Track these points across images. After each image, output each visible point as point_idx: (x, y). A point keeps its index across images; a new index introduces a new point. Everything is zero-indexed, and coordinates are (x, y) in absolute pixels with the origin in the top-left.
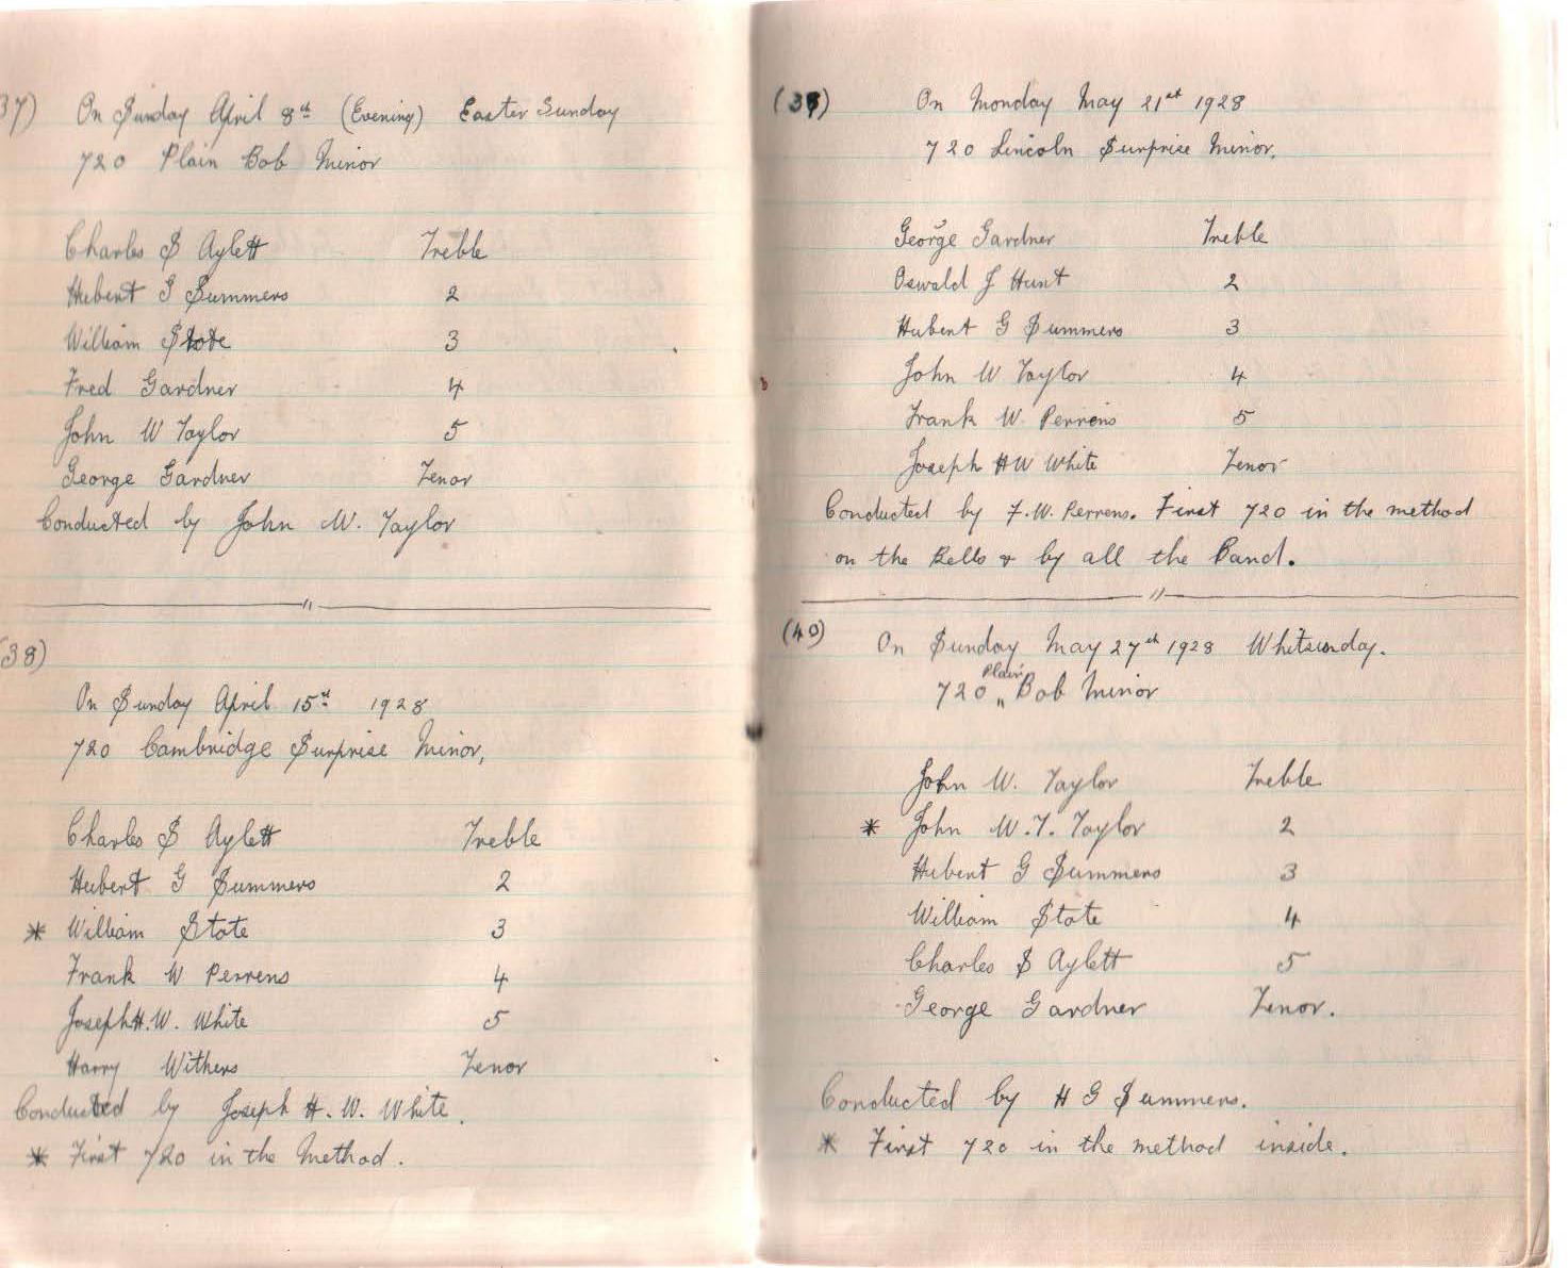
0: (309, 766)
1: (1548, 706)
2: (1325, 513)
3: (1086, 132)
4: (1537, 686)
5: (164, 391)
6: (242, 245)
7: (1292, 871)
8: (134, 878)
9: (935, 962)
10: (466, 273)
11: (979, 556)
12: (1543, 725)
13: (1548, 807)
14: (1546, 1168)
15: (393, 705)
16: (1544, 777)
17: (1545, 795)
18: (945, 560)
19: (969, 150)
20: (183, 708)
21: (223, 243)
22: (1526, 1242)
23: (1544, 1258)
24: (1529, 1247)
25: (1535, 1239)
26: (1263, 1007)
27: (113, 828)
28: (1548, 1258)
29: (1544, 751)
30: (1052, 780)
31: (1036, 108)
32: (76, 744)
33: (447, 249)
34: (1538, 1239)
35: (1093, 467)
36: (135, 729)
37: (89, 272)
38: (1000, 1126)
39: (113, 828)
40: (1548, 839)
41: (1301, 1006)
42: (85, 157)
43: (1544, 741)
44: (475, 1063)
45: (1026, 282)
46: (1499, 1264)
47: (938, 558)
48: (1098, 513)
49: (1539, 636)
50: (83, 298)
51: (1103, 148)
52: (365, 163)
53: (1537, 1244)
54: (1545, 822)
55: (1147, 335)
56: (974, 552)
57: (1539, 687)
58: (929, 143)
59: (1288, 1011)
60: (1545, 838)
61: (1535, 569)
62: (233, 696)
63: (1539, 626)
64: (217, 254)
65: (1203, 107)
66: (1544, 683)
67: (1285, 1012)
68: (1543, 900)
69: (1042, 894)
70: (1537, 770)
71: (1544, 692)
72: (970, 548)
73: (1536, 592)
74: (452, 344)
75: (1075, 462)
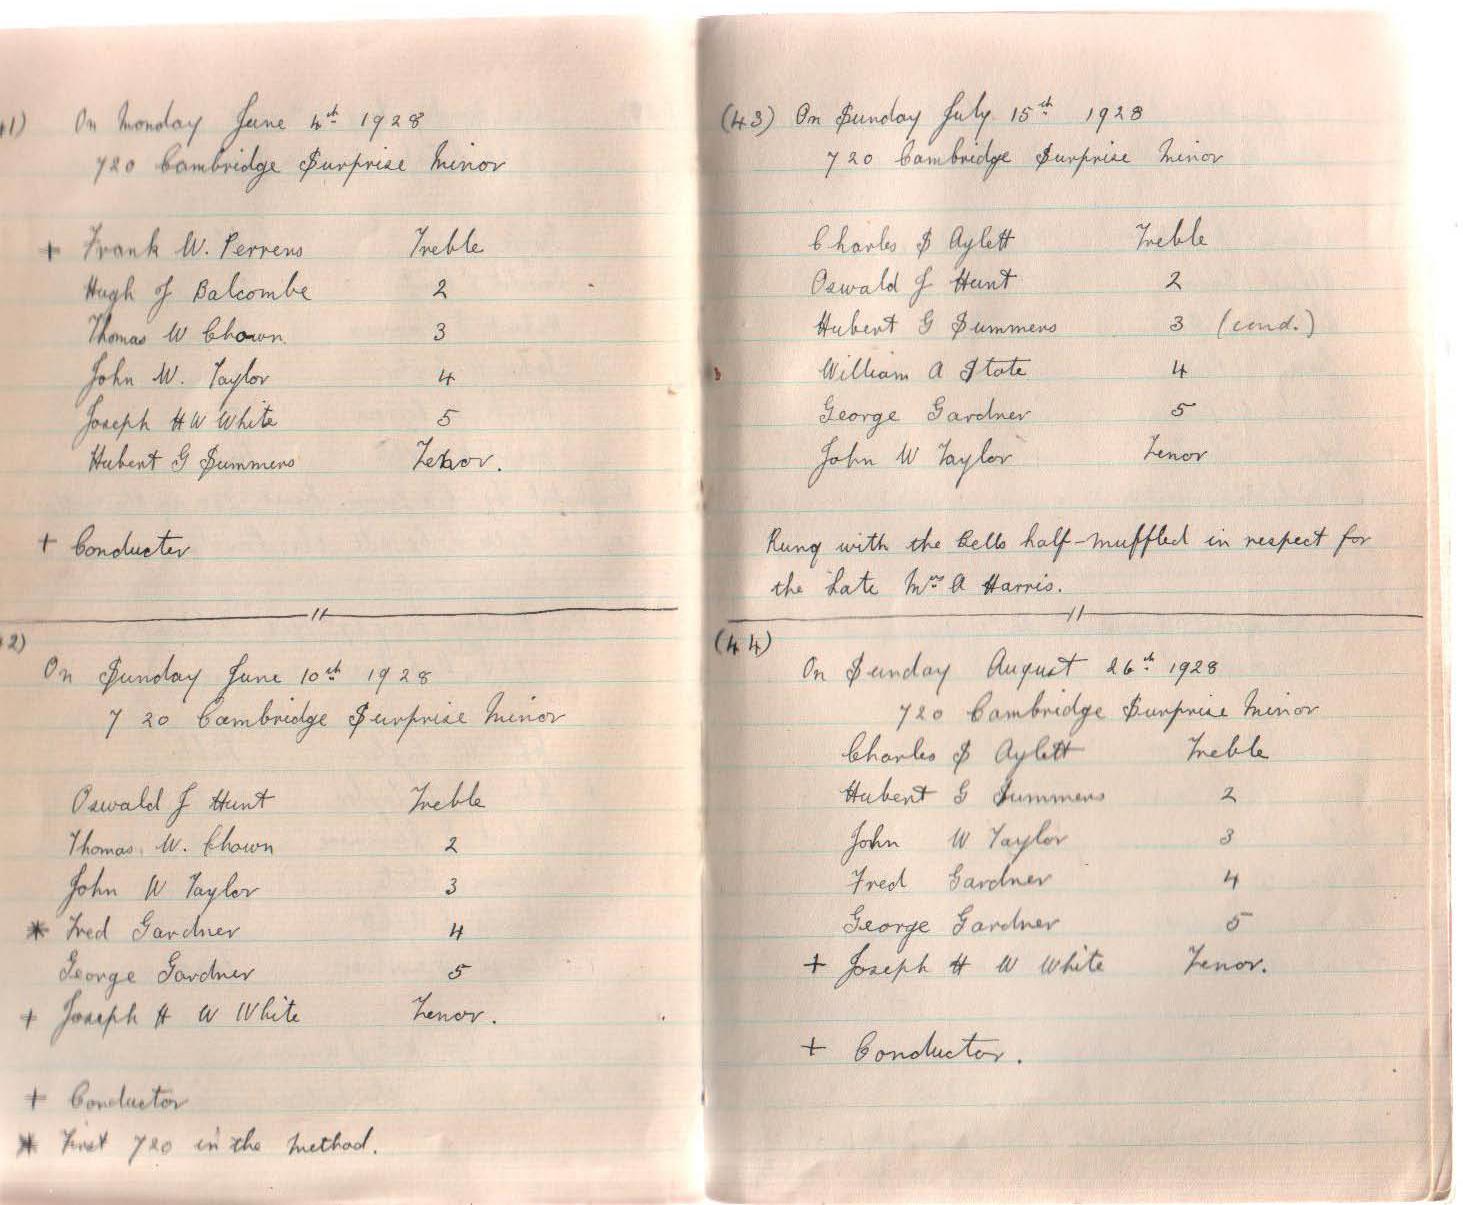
3: (1020, 142)
4: (1438, 657)
5: (222, 382)
6: (994, 238)
7: (1230, 836)
9: (133, 1015)
11: (1000, 541)
12: (1445, 692)
14: (1450, 1108)
16: (1446, 741)
17: (1446, 758)
18: (969, 543)
19: (868, 159)
21: (973, 234)
22: (1429, 1179)
25: (1439, 1174)
26: (1197, 961)
28: (1451, 1193)
31: (904, 123)
40: (1450, 799)
42: (102, 163)
44: (1200, 959)
45: (99, 292)
47: (962, 542)
50: (102, 293)
54: (1446, 781)
55: (1090, 339)
56: (995, 537)
57: (1440, 656)
58: (830, 154)
60: (1447, 798)
61: (1436, 546)
63: (1440, 599)
66: (1445, 652)
68: (1443, 858)
70: (1438, 735)
72: (1061, 528)
73: (1437, 568)
74: (440, 335)
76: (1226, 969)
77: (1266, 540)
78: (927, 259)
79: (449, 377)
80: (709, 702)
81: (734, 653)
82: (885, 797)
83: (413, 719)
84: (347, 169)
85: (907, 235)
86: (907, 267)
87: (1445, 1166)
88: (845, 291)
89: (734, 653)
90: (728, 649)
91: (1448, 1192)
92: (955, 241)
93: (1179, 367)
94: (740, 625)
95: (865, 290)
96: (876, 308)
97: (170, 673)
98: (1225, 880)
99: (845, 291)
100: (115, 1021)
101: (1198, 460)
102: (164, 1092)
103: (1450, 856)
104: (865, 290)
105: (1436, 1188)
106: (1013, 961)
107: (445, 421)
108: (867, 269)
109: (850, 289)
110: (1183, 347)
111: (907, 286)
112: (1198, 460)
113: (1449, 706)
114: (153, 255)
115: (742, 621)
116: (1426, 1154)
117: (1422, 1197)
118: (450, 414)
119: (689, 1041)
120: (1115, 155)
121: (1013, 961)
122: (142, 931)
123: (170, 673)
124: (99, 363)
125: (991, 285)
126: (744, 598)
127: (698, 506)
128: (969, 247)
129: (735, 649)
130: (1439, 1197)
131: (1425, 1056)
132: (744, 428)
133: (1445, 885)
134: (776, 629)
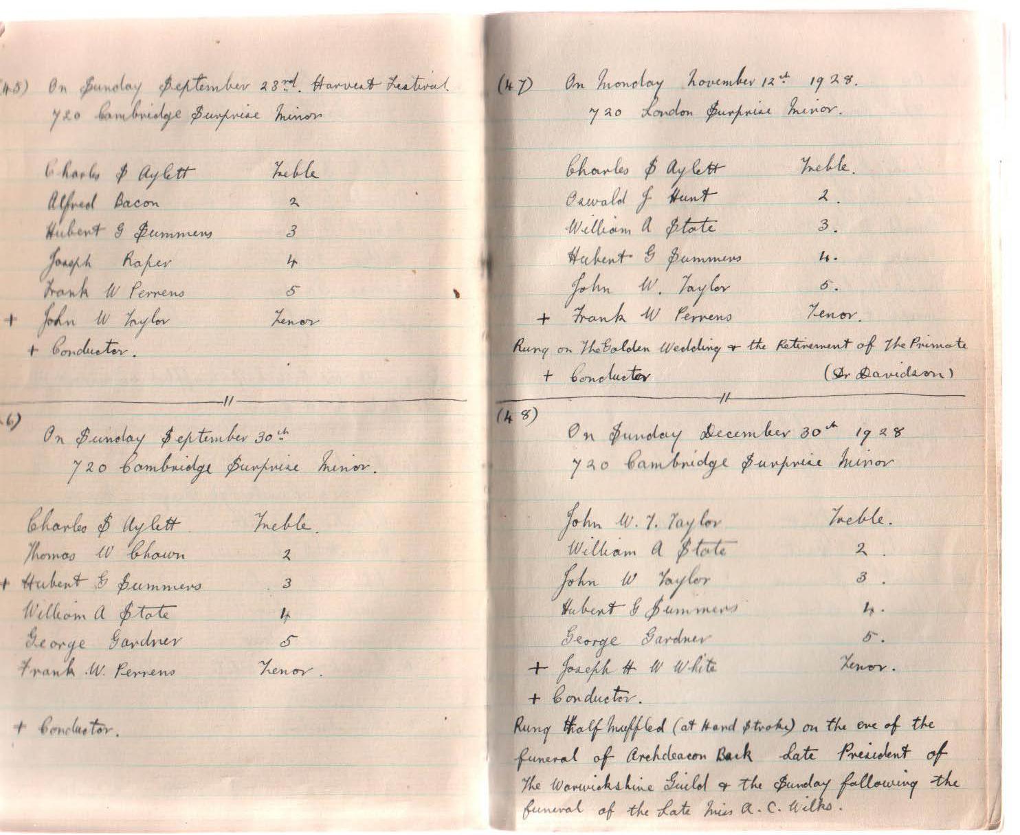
0: (242, 479)
1: (1000, 468)
2: (705, 756)
8: (77, 578)
10: (300, 187)
12: (997, 481)
13: (1001, 534)
14: (1000, 766)
16: (998, 514)
17: (998, 525)
24: (988, 818)
25: (992, 813)
30: (673, 520)
37: (65, 186)
42: (56, 114)
43: (998, 492)
46: (973, 829)
51: (162, 86)
52: (684, 112)
53: (994, 814)
54: (998, 542)
60: (999, 553)
63: (994, 416)
65: (816, 84)
69: (646, 626)
71: (998, 460)
78: (652, 180)
80: (491, 488)
81: (509, 422)
85: (637, 165)
86: (635, 185)
88: (591, 203)
89: (509, 422)
90: (505, 420)
91: (999, 823)
92: (671, 170)
94: (515, 403)
95: (604, 203)
96: (609, 216)
97: (124, 85)
98: (821, 259)
99: (591, 203)
102: (98, 724)
103: (1001, 593)
104: (604, 203)
105: (990, 822)
108: (607, 187)
109: (595, 201)
110: (826, 242)
111: (635, 199)
113: (1000, 490)
114: (84, 295)
115: (516, 401)
116: (984, 799)
117: (980, 827)
119: (478, 721)
123: (124, 85)
124: (49, 310)
126: (515, 266)
128: (681, 172)
129: (510, 420)
130: (992, 828)
131: (984, 729)
132: (519, 443)
133: (997, 613)
134: (540, 405)
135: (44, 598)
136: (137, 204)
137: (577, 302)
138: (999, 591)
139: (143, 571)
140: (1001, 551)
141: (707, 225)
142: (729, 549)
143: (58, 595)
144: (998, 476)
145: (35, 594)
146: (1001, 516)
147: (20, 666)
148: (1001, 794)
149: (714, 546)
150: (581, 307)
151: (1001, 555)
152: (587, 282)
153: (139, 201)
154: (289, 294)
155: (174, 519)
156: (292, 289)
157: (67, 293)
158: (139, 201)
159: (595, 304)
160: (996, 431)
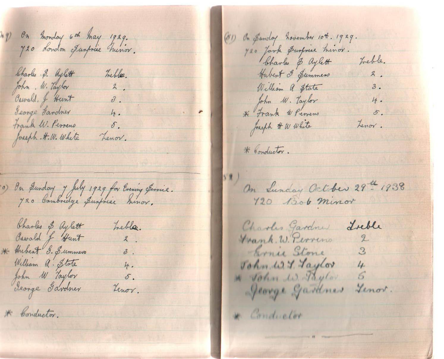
1: (433, 203)
12: (431, 208)
15: (344, 37)
16: (432, 223)
20: (52, 190)
23: (431, 357)
27: (31, 222)
28: (432, 357)
29: (431, 215)
32: (21, 199)
33: (111, 74)
34: (430, 351)
35: (309, 127)
36: (41, 194)
38: (101, 195)
39: (31, 222)
41: (378, 289)
43: (432, 213)
45: (20, 251)
48: (262, 152)
49: (430, 183)
54: (432, 234)
59: (273, 255)
62: (252, 223)
64: (57, 88)
67: (272, 255)
75: (302, 126)
76: (316, 255)
77: (310, 50)
79: (128, 265)
82: (308, 38)
83: (303, 51)
84: (301, 52)
87: (431, 347)
88: (25, 239)
91: (432, 356)
93: (361, 264)
100: (266, 128)
101: (373, 127)
106: (289, 125)
107: (127, 277)
112: (373, 127)
113: (433, 212)
118: (129, 275)
120: (359, 226)
121: (289, 125)
122: (290, 75)
125: (66, 100)
127: (209, 191)
133: (431, 266)
135: (21, 256)
136: (43, 316)
137: (259, 107)
138: (432, 256)
139: (68, 246)
140: (433, 238)
141: (315, 87)
142: (318, 87)
143: (28, 256)
144: (432, 206)
145: (19, 256)
146: (433, 224)
147: (11, 310)
148: (432, 345)
149: (313, 87)
150: (260, 109)
151: (433, 240)
152: (263, 99)
153: (44, 315)
154: (126, 278)
155: (80, 224)
156: (128, 276)
157: (25, 127)
158: (44, 315)
159: (266, 108)
160: (431, 187)
